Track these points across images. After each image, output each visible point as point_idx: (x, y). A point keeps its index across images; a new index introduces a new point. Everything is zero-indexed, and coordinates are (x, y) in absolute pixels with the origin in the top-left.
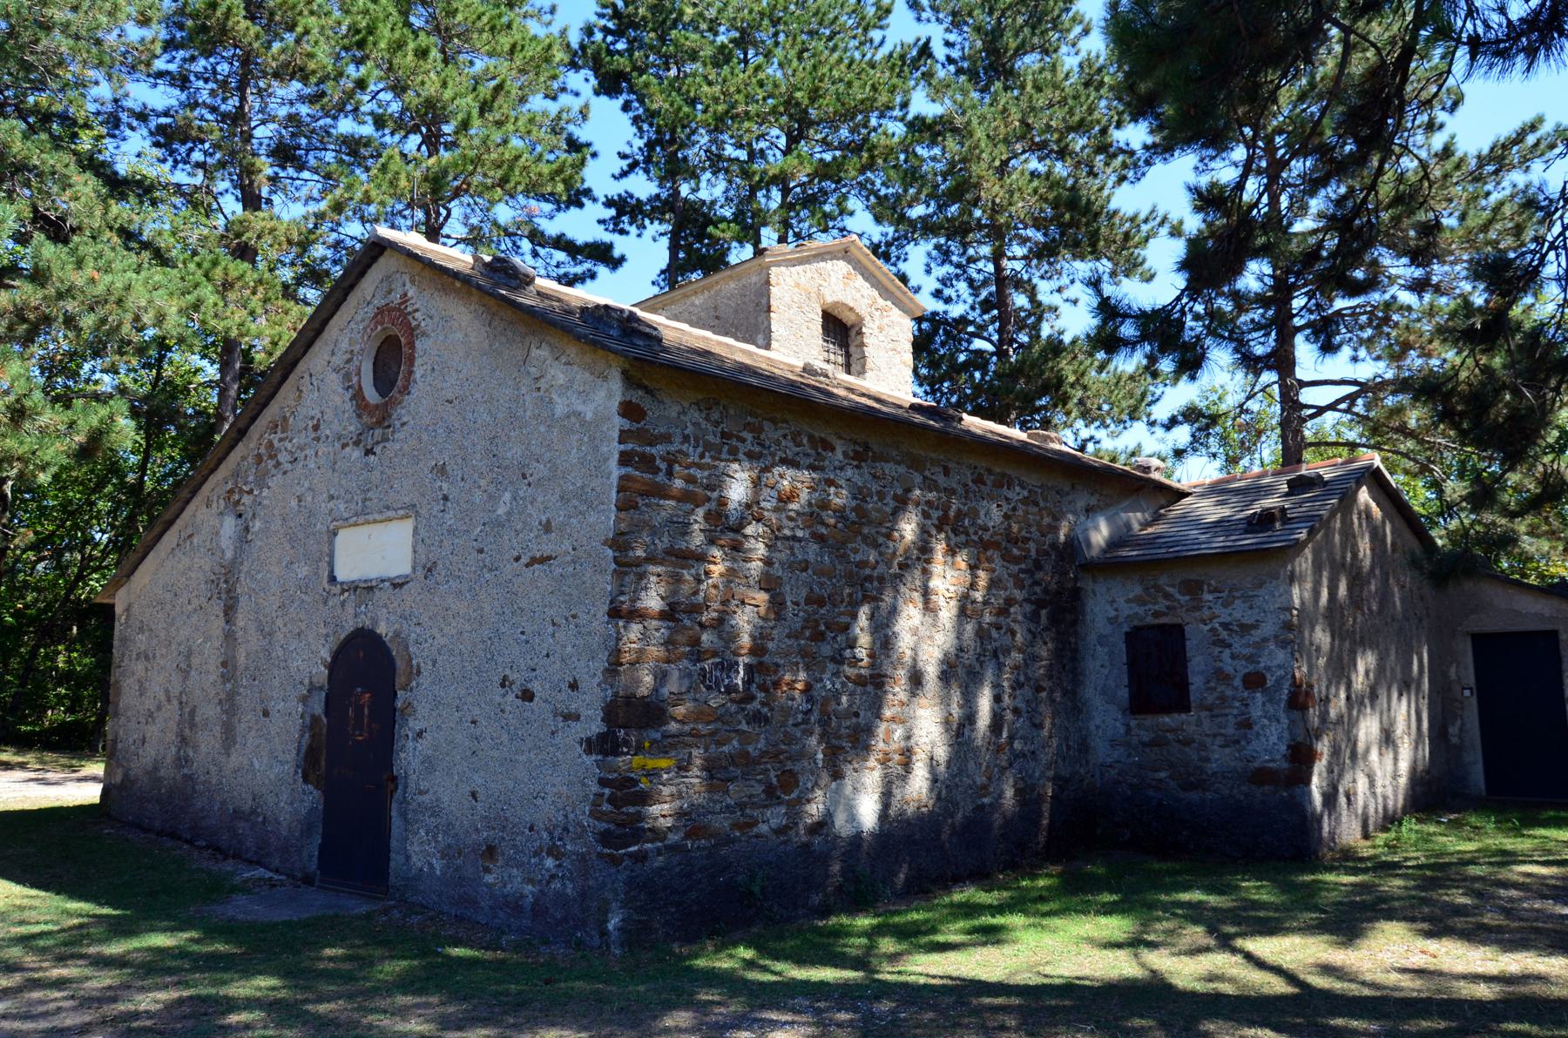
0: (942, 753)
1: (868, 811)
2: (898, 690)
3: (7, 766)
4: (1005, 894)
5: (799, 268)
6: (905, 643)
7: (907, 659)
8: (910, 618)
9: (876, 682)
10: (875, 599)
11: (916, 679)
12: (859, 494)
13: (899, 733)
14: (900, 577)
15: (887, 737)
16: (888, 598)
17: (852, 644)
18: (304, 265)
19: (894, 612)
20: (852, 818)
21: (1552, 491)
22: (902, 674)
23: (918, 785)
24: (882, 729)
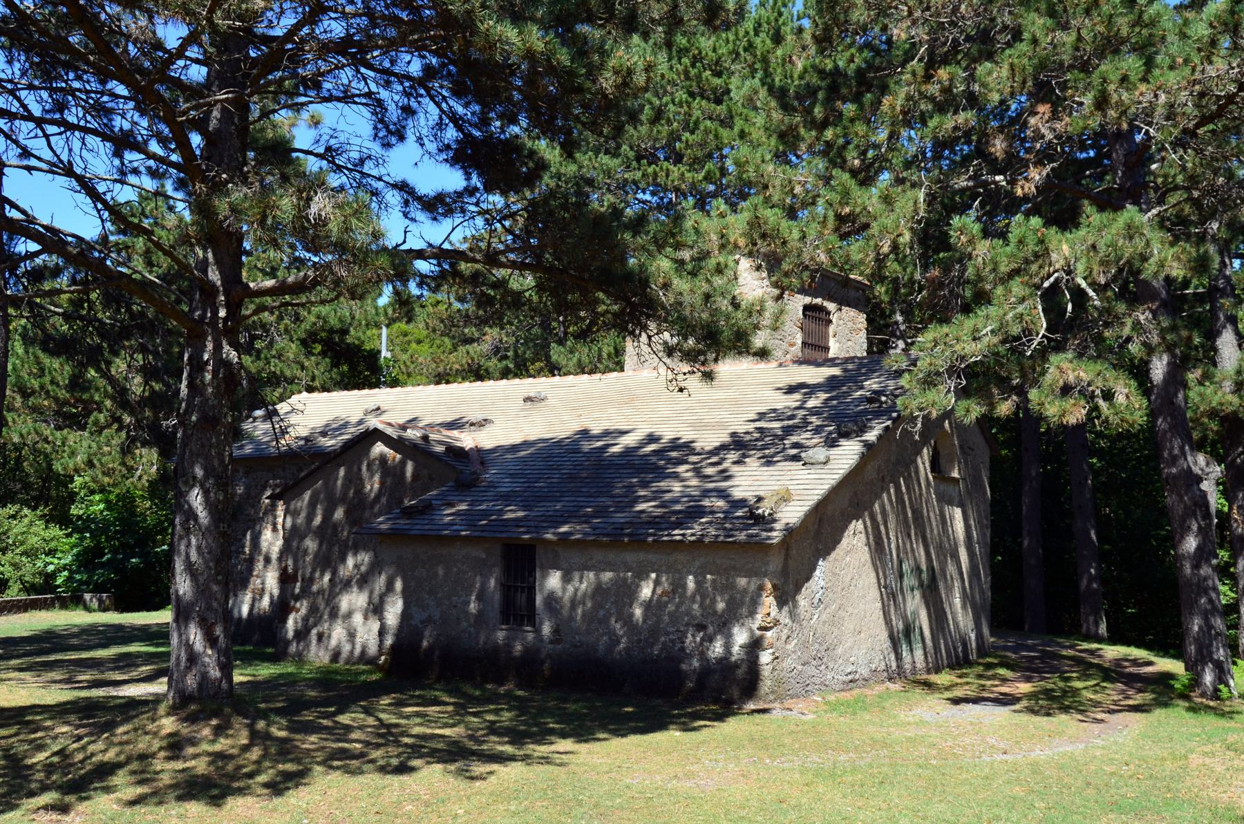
0: (276, 592)
1: (245, 610)
2: (260, 565)
3: (2, 680)
4: (209, 338)
5: (882, 620)
6: (264, 545)
7: (264, 550)
8: (267, 535)
9: (251, 561)
10: (253, 529)
11: (267, 560)
12: (247, 488)
13: (259, 581)
14: (262, 519)
15: (255, 582)
16: (258, 528)
17: (243, 547)
18: (524, 305)
19: (260, 533)
20: (240, 611)
21: (1238, 230)
22: (261, 558)
23: (266, 602)
24: (252, 579)
